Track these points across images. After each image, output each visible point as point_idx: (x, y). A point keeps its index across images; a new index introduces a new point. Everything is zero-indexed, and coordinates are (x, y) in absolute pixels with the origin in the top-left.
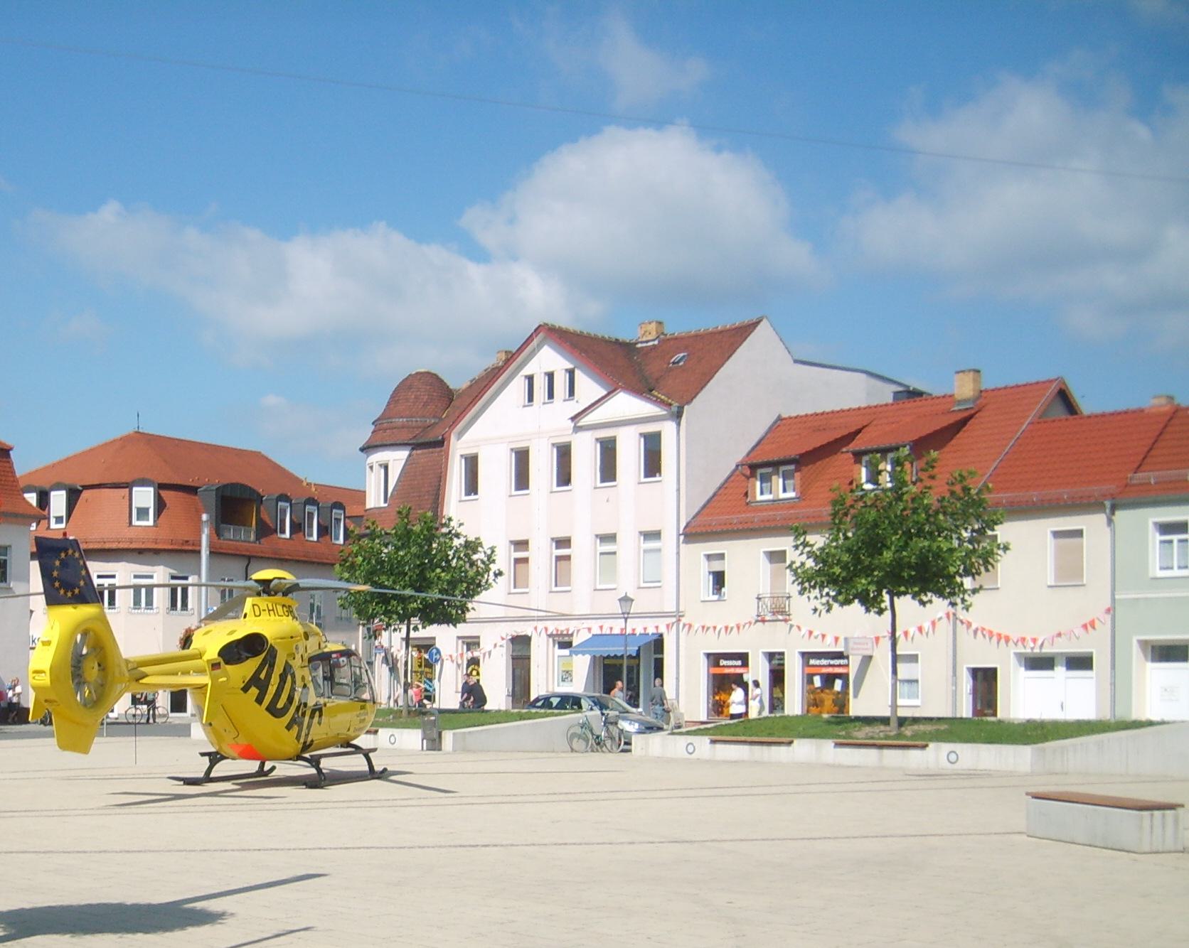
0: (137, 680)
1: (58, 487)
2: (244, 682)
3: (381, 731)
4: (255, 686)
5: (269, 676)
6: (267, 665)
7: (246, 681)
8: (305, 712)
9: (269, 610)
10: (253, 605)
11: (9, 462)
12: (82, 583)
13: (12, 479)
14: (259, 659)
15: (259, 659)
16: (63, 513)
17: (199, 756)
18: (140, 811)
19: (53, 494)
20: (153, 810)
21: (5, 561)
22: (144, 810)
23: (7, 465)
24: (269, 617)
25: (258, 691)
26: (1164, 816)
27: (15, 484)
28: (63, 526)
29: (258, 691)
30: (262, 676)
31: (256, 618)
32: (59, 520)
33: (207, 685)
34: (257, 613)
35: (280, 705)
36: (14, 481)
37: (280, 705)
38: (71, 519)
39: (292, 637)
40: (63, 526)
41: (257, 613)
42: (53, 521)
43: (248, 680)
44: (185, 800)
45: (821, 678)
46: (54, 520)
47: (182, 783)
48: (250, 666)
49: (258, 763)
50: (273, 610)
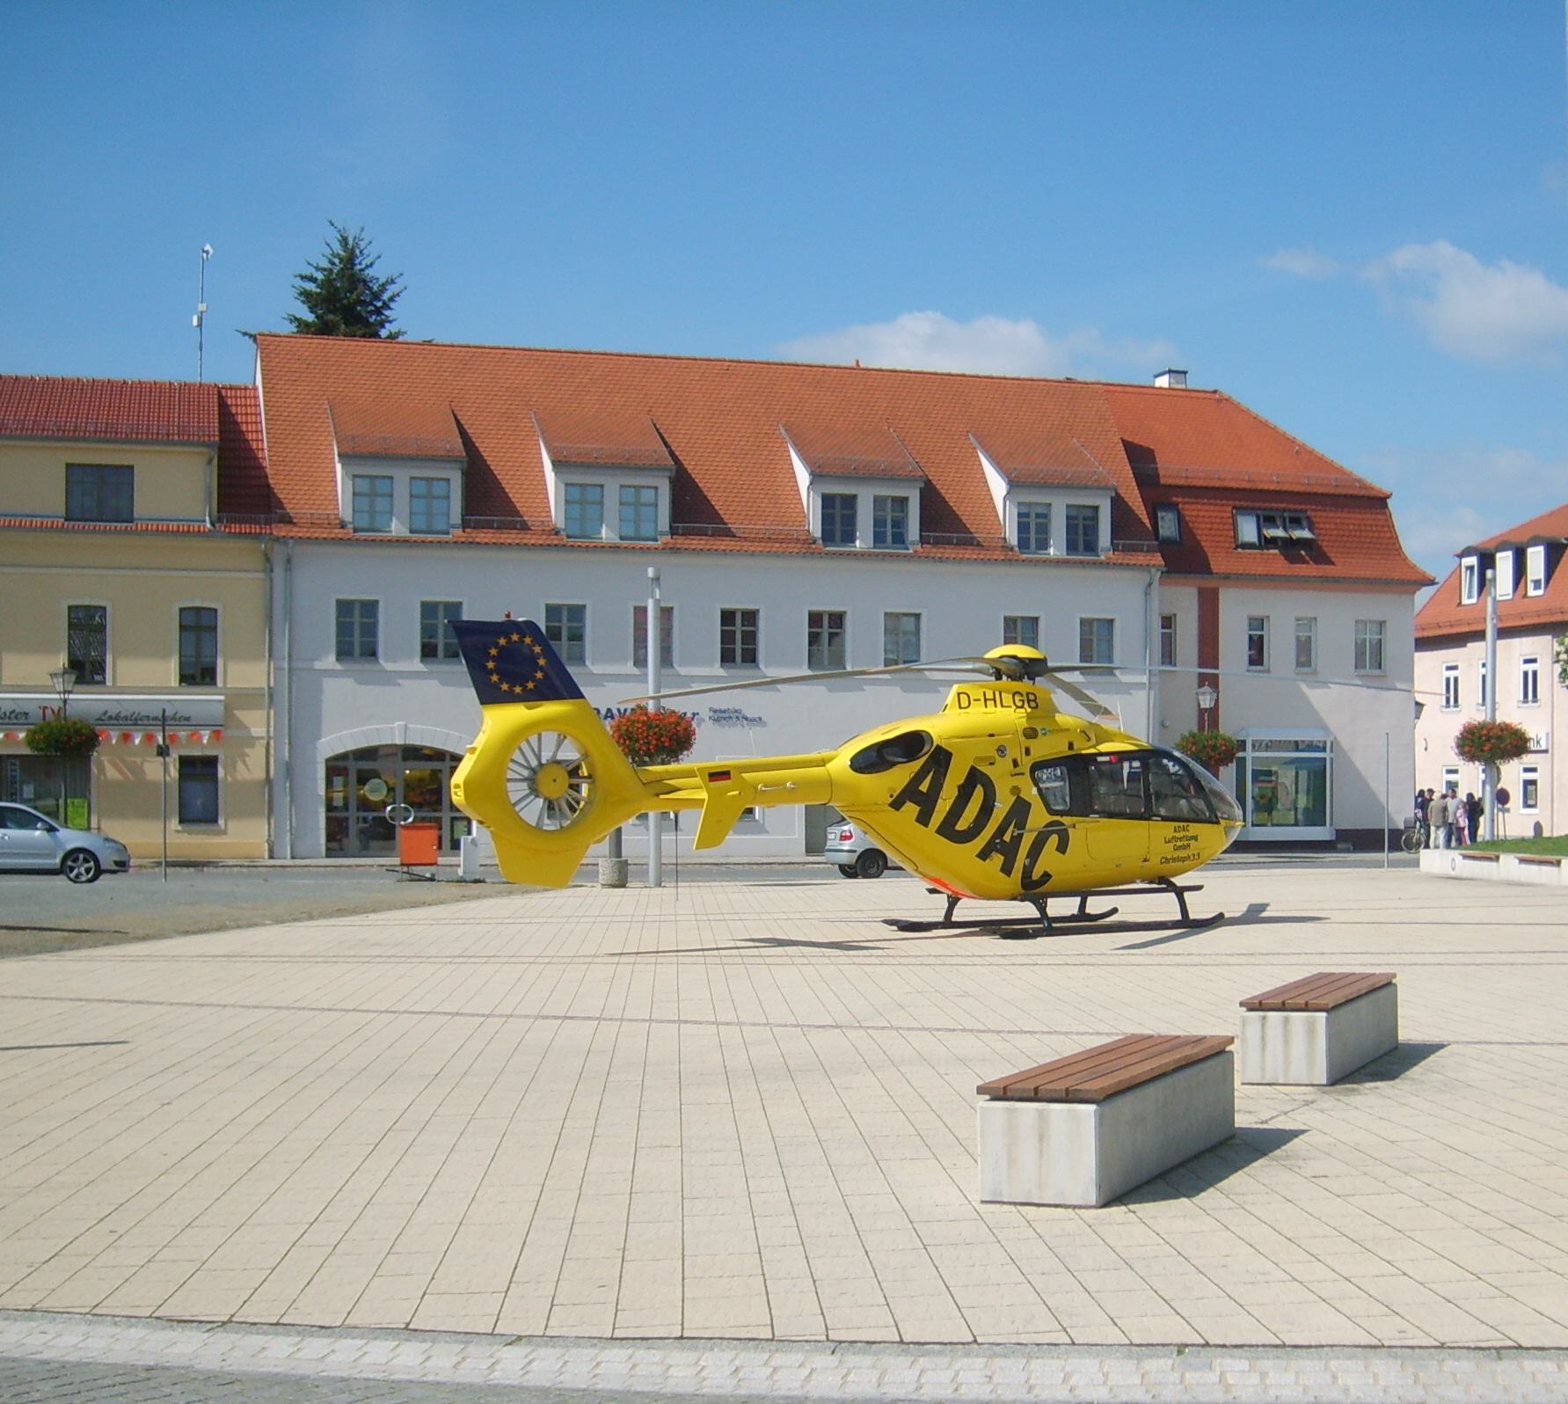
0: (658, 795)
1: (1534, 542)
2: (891, 796)
3: (1502, 857)
4: (911, 801)
5: (937, 787)
6: (931, 774)
7: (895, 795)
8: (1021, 836)
9: (986, 700)
10: (959, 694)
11: (1385, 514)
12: (491, 665)
13: (1388, 535)
14: (917, 765)
15: (917, 765)
16: (1541, 575)
17: (927, 892)
18: (1132, 959)
19: (1530, 550)
20: (856, 960)
21: (1261, 637)
22: (1141, 960)
23: (1383, 517)
24: (984, 710)
25: (918, 808)
26: (1286, 1020)
27: (1392, 541)
28: (1540, 592)
29: (918, 808)
30: (924, 787)
31: (962, 711)
32: (1537, 584)
33: (703, 800)
34: (964, 704)
35: (962, 825)
36: (1392, 537)
37: (962, 825)
38: (1552, 581)
39: (992, 735)
40: (1540, 592)
41: (964, 704)
42: (1530, 586)
43: (898, 792)
44: (787, 948)
45: (1016, 801)
46: (1533, 585)
47: (895, 928)
48: (900, 776)
49: (1078, 900)
50: (994, 700)
